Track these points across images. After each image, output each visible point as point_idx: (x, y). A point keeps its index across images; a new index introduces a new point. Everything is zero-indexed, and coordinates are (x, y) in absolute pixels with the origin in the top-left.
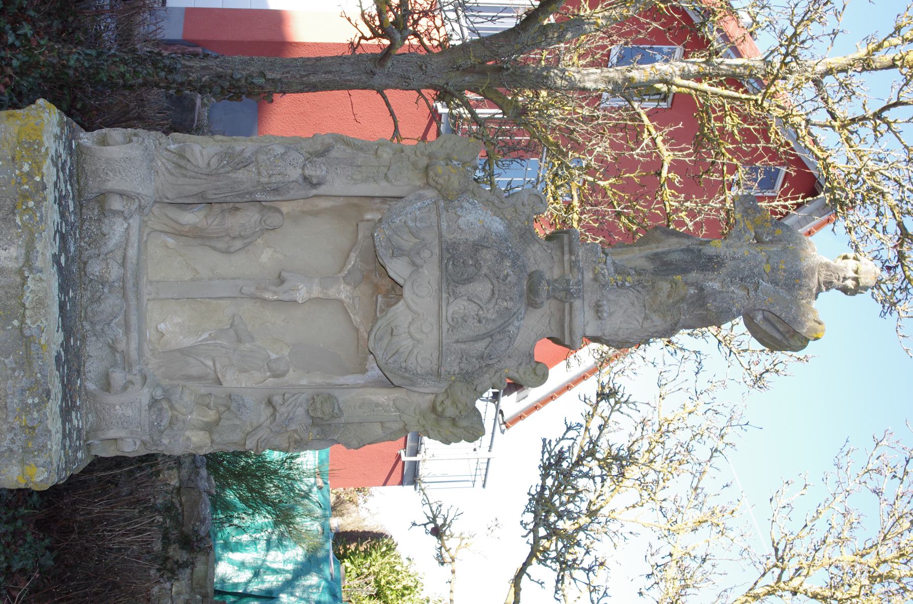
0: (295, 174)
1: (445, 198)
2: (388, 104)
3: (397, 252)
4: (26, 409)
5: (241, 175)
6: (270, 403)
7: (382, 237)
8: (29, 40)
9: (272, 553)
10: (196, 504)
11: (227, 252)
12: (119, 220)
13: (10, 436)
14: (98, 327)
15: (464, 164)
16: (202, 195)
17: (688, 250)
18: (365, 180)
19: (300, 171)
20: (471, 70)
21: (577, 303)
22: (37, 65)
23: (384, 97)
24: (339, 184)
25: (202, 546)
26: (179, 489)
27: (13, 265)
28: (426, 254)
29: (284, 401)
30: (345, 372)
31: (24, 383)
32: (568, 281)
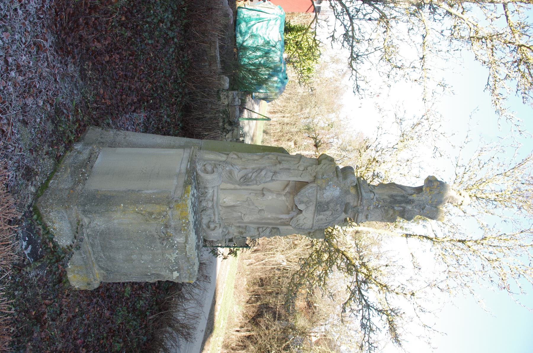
3: (301, 202)
17: (403, 196)
18: (294, 176)
30: (283, 213)
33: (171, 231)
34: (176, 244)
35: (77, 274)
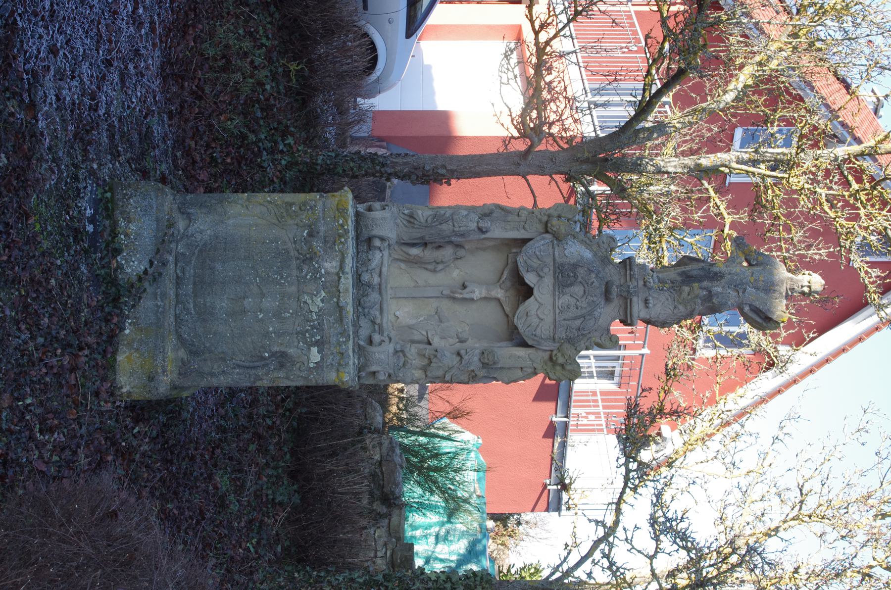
0: (473, 226)
1: (557, 239)
2: (529, 185)
4: (339, 344)
5: (444, 227)
6: (459, 354)
7: (521, 260)
8: (291, 147)
9: (440, 547)
10: (393, 472)
11: (434, 271)
12: (378, 252)
13: (331, 357)
14: (366, 310)
15: (568, 220)
16: (422, 238)
17: (703, 268)
19: (475, 224)
20: (586, 161)
21: (635, 299)
22: (297, 164)
23: (527, 181)
24: (498, 232)
25: (397, 502)
26: (380, 462)
27: (333, 271)
28: (546, 270)
29: (467, 353)
31: (339, 330)
32: (629, 286)
33: (317, 245)
34: (321, 276)
35: (137, 350)
